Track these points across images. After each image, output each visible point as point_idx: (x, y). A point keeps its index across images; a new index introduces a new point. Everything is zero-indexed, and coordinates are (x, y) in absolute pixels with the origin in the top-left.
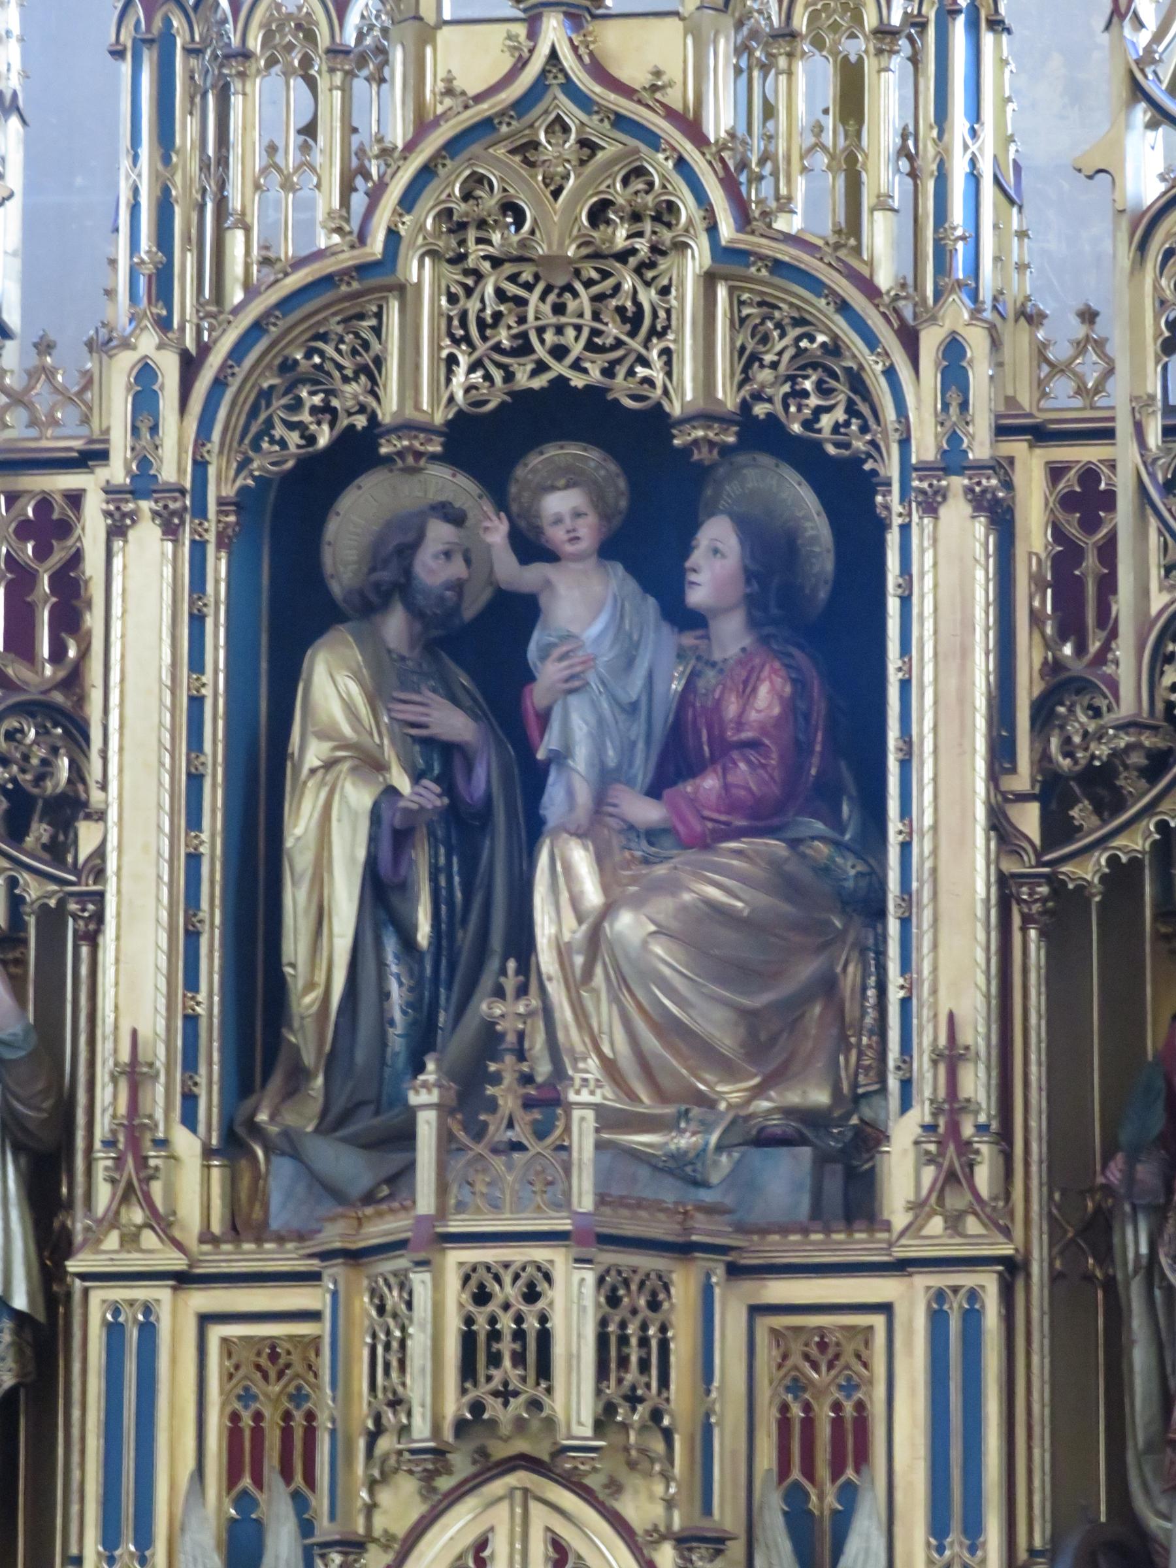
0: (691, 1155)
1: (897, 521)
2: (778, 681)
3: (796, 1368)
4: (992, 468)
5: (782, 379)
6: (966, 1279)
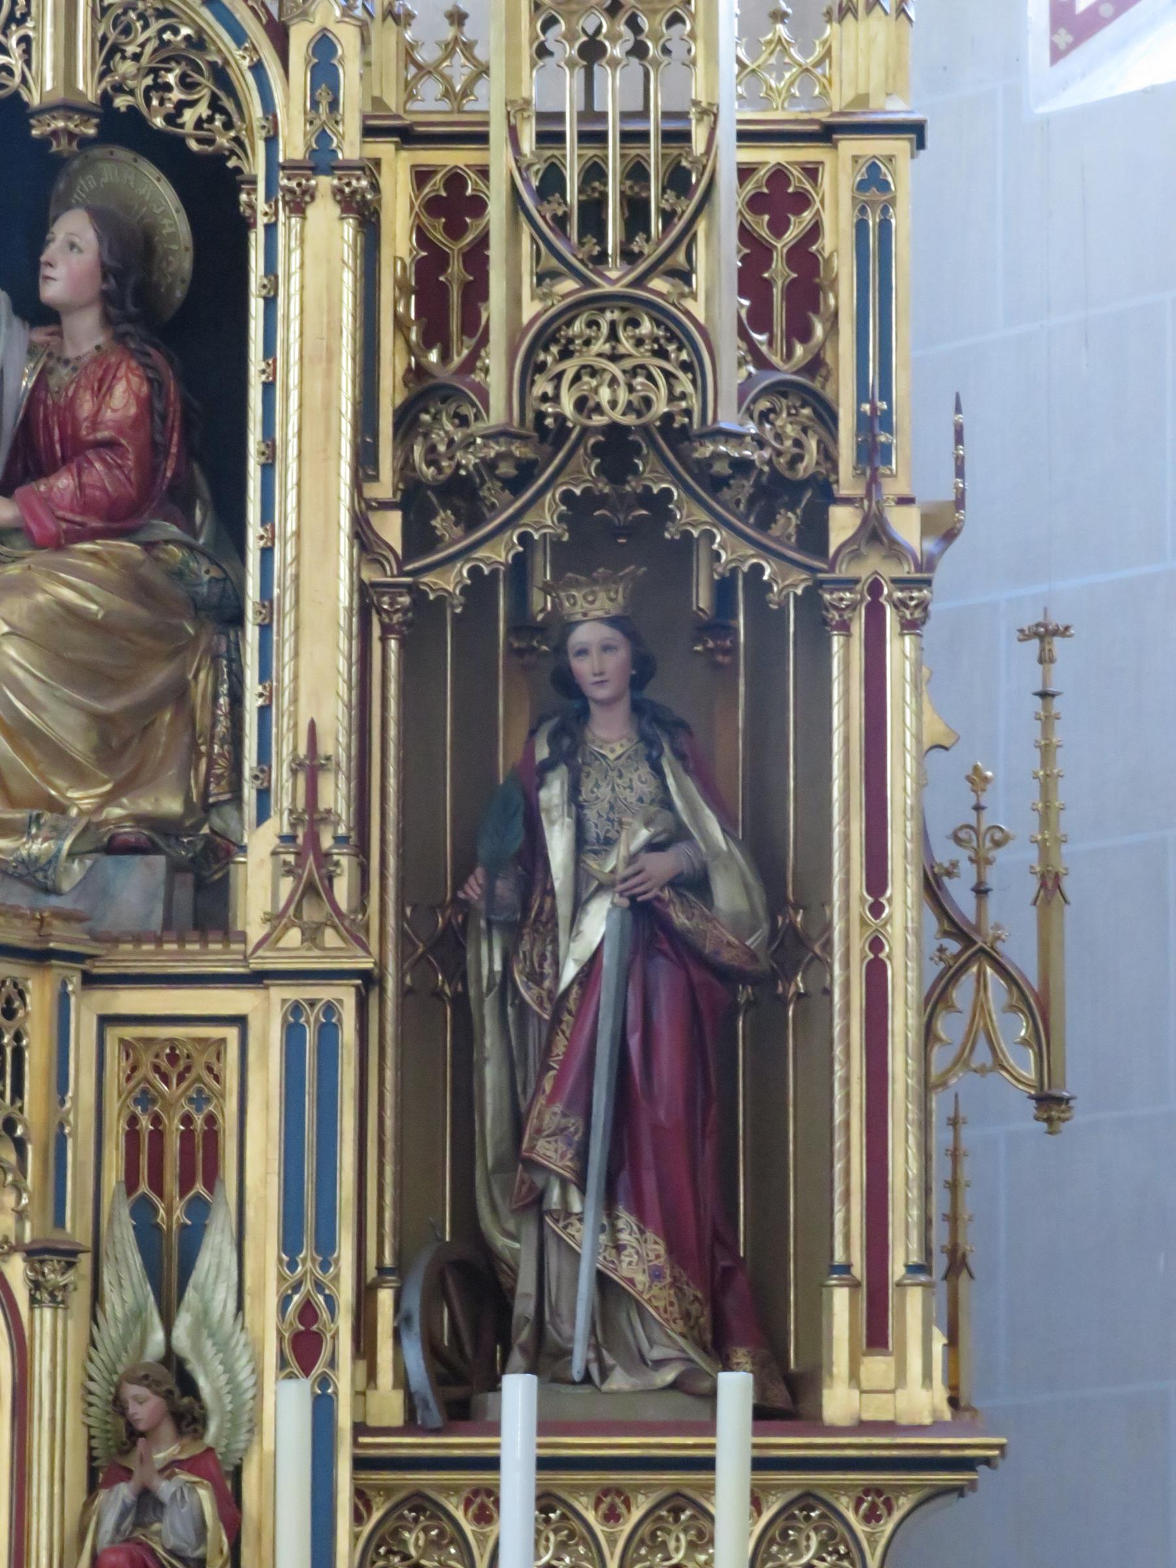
0: (43, 861)
1: (262, 221)
2: (135, 380)
3: (146, 1079)
4: (362, 169)
5: (143, 72)
6: (324, 993)
